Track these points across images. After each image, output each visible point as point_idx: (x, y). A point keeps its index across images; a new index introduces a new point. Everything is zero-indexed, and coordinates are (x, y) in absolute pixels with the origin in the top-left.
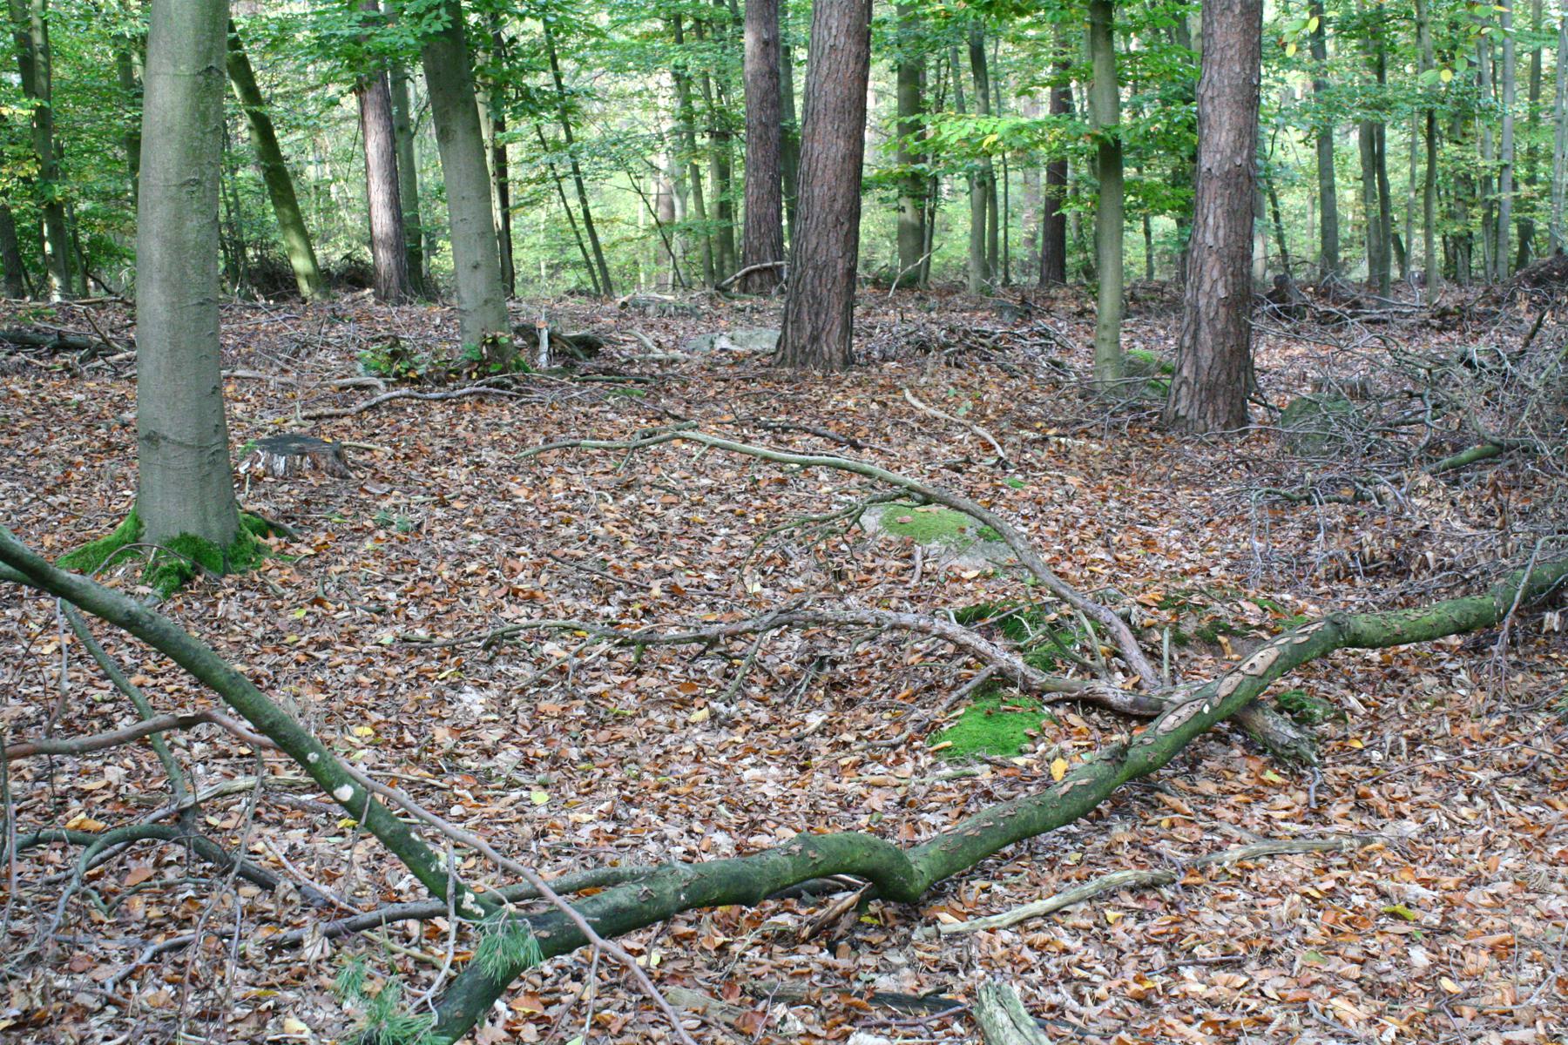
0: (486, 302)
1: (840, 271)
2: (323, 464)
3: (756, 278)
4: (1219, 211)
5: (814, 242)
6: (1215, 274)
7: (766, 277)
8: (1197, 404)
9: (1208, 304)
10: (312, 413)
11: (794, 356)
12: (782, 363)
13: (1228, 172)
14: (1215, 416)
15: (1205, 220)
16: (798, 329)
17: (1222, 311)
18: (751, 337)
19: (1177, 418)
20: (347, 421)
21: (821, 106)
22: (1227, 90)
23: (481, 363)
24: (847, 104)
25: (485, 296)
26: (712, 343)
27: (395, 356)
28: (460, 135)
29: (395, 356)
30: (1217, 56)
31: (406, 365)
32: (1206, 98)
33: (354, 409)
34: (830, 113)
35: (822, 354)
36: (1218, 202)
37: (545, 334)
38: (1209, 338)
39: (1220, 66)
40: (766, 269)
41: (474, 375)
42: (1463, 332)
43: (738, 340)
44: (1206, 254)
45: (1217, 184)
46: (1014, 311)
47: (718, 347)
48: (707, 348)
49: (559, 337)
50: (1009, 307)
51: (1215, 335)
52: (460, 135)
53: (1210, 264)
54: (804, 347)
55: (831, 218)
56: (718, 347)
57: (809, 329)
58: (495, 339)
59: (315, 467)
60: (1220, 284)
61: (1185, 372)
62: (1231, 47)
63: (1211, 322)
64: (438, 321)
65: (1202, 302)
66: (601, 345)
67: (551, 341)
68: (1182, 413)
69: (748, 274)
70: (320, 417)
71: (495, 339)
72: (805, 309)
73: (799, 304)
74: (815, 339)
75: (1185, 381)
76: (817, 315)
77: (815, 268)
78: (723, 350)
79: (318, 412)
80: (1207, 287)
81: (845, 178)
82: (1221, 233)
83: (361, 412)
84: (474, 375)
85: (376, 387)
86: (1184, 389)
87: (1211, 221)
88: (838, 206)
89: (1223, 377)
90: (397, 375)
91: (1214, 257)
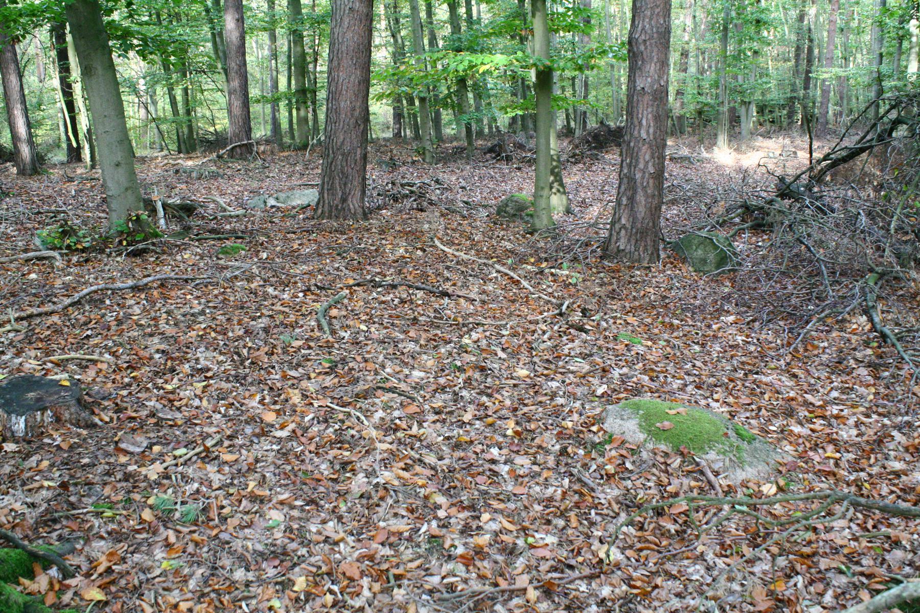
0: (127, 189)
1: (358, 157)
2: (67, 415)
3: (238, 150)
4: (650, 116)
5: (342, 137)
6: (647, 157)
7: (244, 149)
8: (633, 242)
9: (643, 178)
10: (23, 314)
11: (330, 212)
12: (322, 216)
13: (656, 91)
14: (646, 249)
15: (640, 123)
16: (333, 194)
17: (651, 181)
18: (288, 197)
19: (619, 251)
20: (55, 318)
21: (344, 48)
22: (655, 35)
23: (129, 234)
24: (361, 47)
25: (126, 184)
26: (265, 202)
27: (65, 234)
28: (100, 71)
29: (65, 234)
30: (648, 13)
31: (74, 239)
32: (640, 41)
33: (60, 306)
34: (351, 53)
35: (349, 210)
36: (650, 110)
37: (159, 205)
38: (643, 199)
39: (651, 19)
40: (243, 145)
41: (125, 243)
42: (584, 164)
43: (281, 199)
44: (640, 145)
45: (647, 98)
46: (387, 164)
47: (269, 205)
48: (262, 206)
49: (169, 205)
50: (384, 162)
51: (647, 196)
52: (100, 71)
53: (643, 151)
54: (337, 206)
55: (353, 121)
56: (269, 205)
57: (340, 194)
58: (138, 216)
59: (58, 419)
60: (650, 164)
61: (623, 221)
62: (657, 6)
63: (644, 189)
64: (73, 193)
65: (638, 176)
66: (195, 209)
67: (164, 209)
68: (622, 247)
69: (233, 148)
70: (31, 316)
71: (138, 216)
72: (337, 181)
73: (332, 178)
74: (344, 200)
75: (624, 227)
76: (345, 184)
77: (343, 154)
78: (272, 207)
79: (29, 312)
80: (641, 166)
81: (360, 95)
82: (651, 130)
83: (66, 308)
84: (125, 243)
85: (54, 258)
86: (623, 232)
87: (644, 122)
88: (357, 113)
89: (651, 224)
90: (68, 247)
91: (646, 146)
